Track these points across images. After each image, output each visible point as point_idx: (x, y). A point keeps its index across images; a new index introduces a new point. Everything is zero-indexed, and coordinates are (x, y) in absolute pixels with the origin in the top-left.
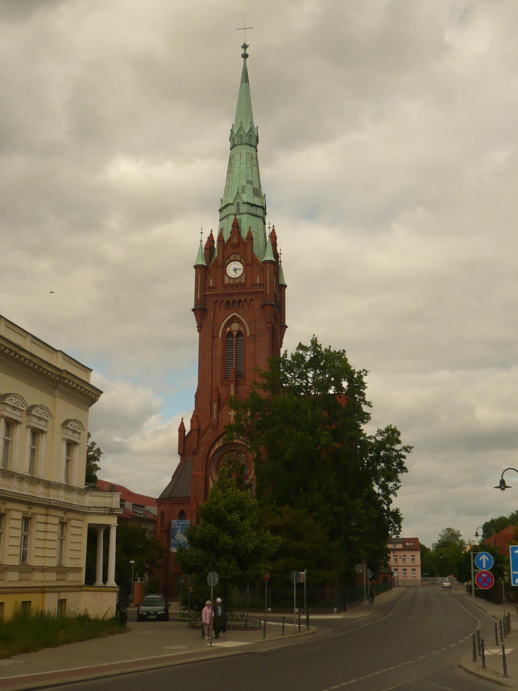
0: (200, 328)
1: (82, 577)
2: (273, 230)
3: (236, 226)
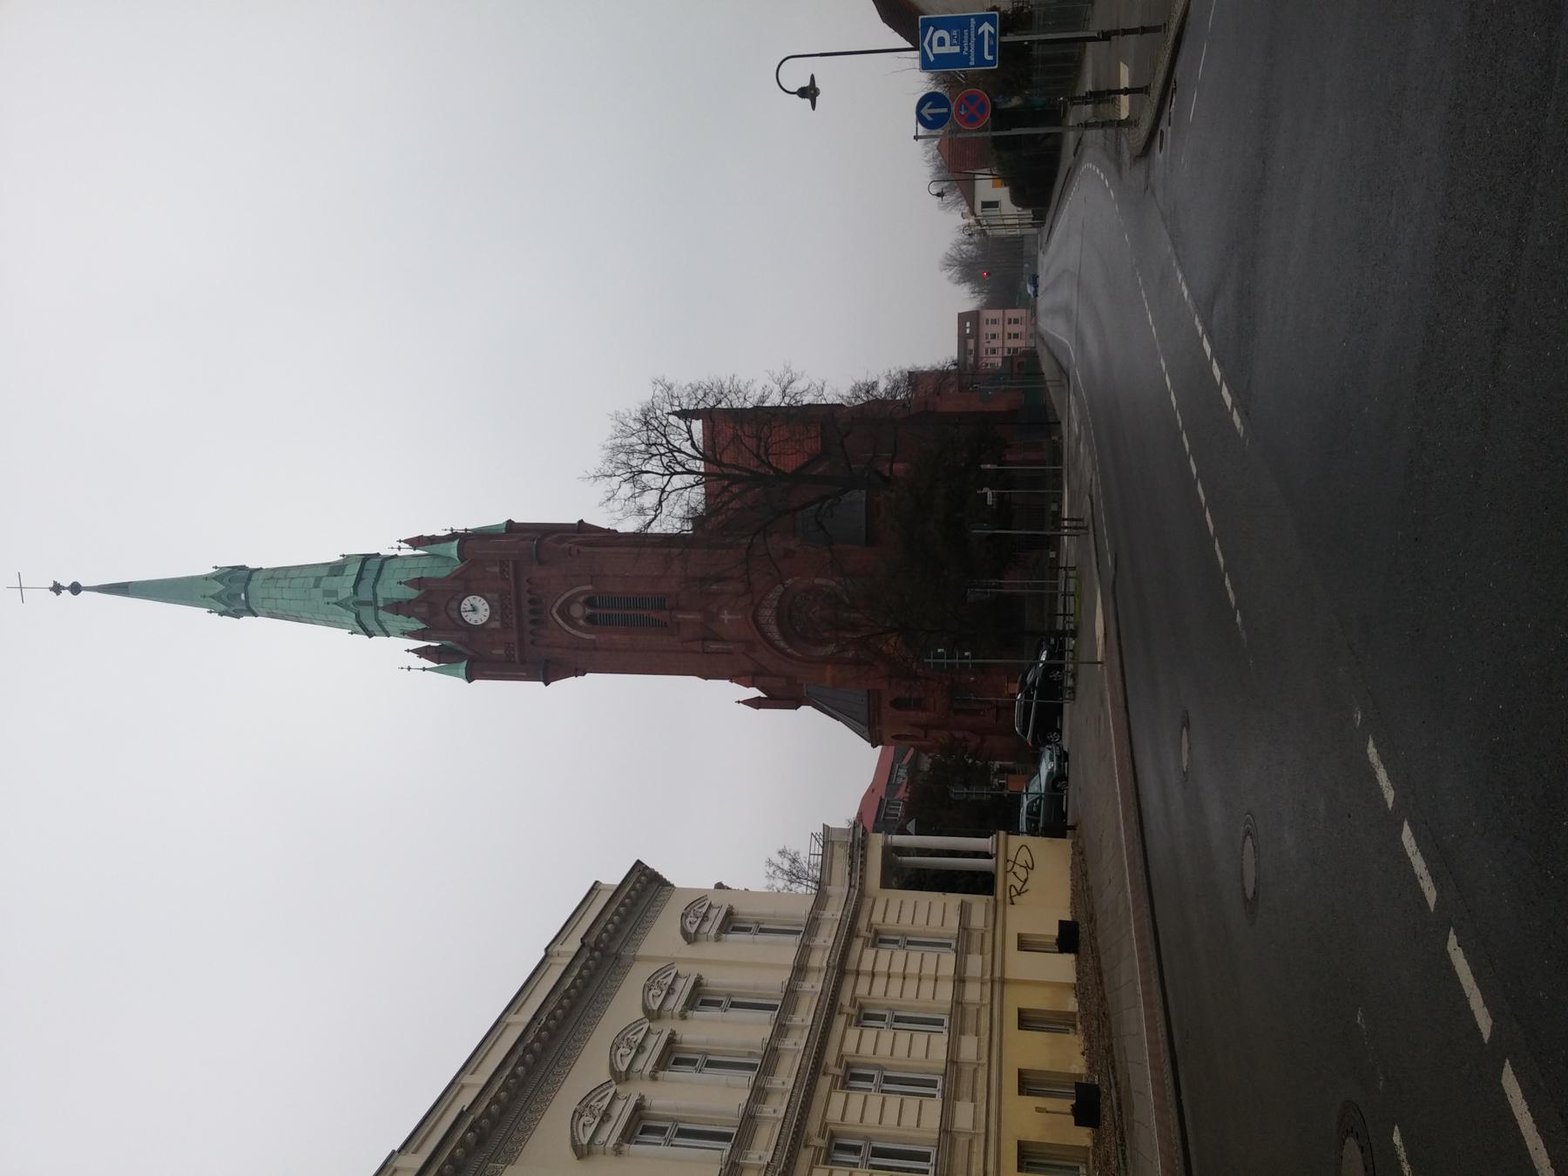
0: (579, 671)
1: (979, 903)
2: (406, 541)
3: (397, 607)
